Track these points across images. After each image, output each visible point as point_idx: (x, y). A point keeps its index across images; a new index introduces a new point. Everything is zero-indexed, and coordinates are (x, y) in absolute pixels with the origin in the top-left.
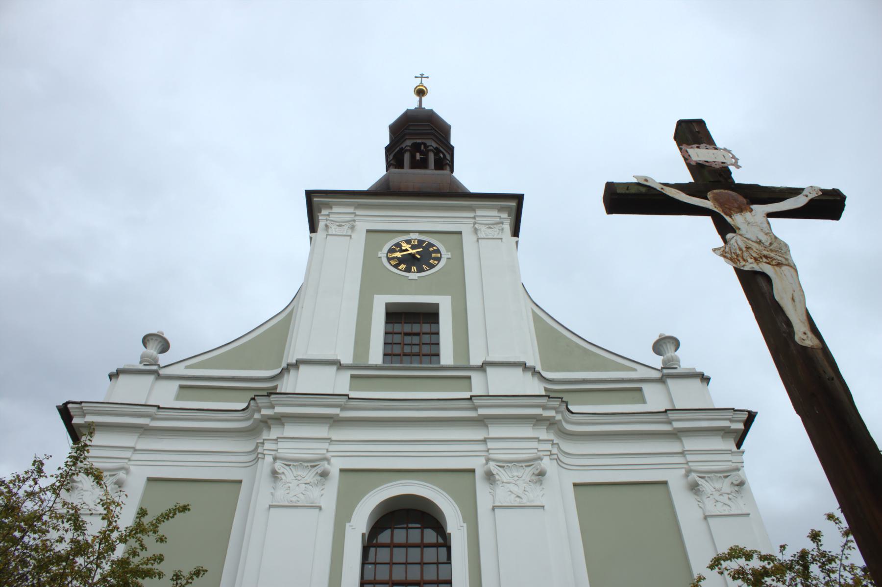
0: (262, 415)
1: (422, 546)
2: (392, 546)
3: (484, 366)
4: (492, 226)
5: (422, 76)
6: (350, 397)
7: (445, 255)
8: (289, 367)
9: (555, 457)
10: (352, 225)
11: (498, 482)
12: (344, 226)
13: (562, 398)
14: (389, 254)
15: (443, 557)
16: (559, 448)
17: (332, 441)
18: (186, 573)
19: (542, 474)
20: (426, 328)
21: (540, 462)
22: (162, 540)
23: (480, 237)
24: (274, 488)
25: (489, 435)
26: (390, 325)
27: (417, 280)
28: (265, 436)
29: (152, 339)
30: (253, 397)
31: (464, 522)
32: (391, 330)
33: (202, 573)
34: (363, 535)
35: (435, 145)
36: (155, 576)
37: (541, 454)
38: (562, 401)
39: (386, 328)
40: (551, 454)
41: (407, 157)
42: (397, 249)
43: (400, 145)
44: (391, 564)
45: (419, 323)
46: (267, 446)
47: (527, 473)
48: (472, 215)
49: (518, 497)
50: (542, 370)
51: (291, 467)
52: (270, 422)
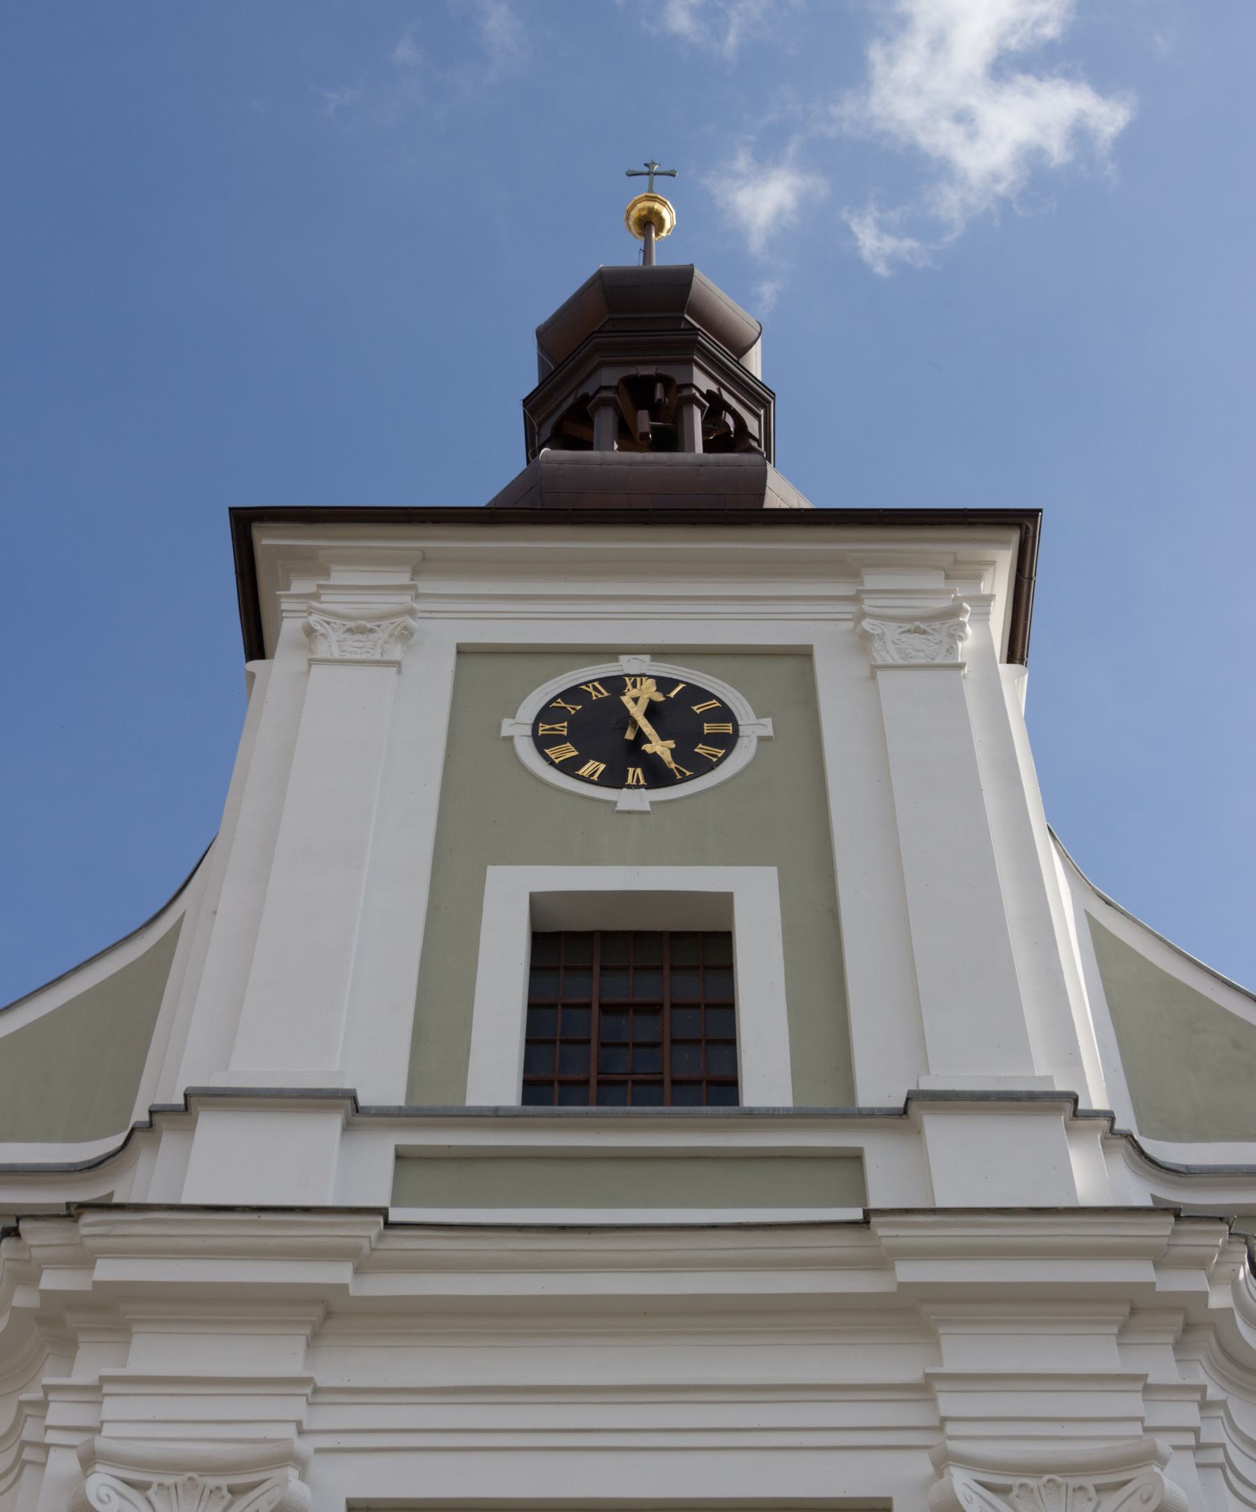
0: (45, 1294)
3: (913, 1106)
9: (1218, 1456)
12: (371, 631)
17: (317, 1391)
23: (880, 662)
27: (646, 813)
43: (576, 388)
46: (59, 1413)
51: (150, 1493)
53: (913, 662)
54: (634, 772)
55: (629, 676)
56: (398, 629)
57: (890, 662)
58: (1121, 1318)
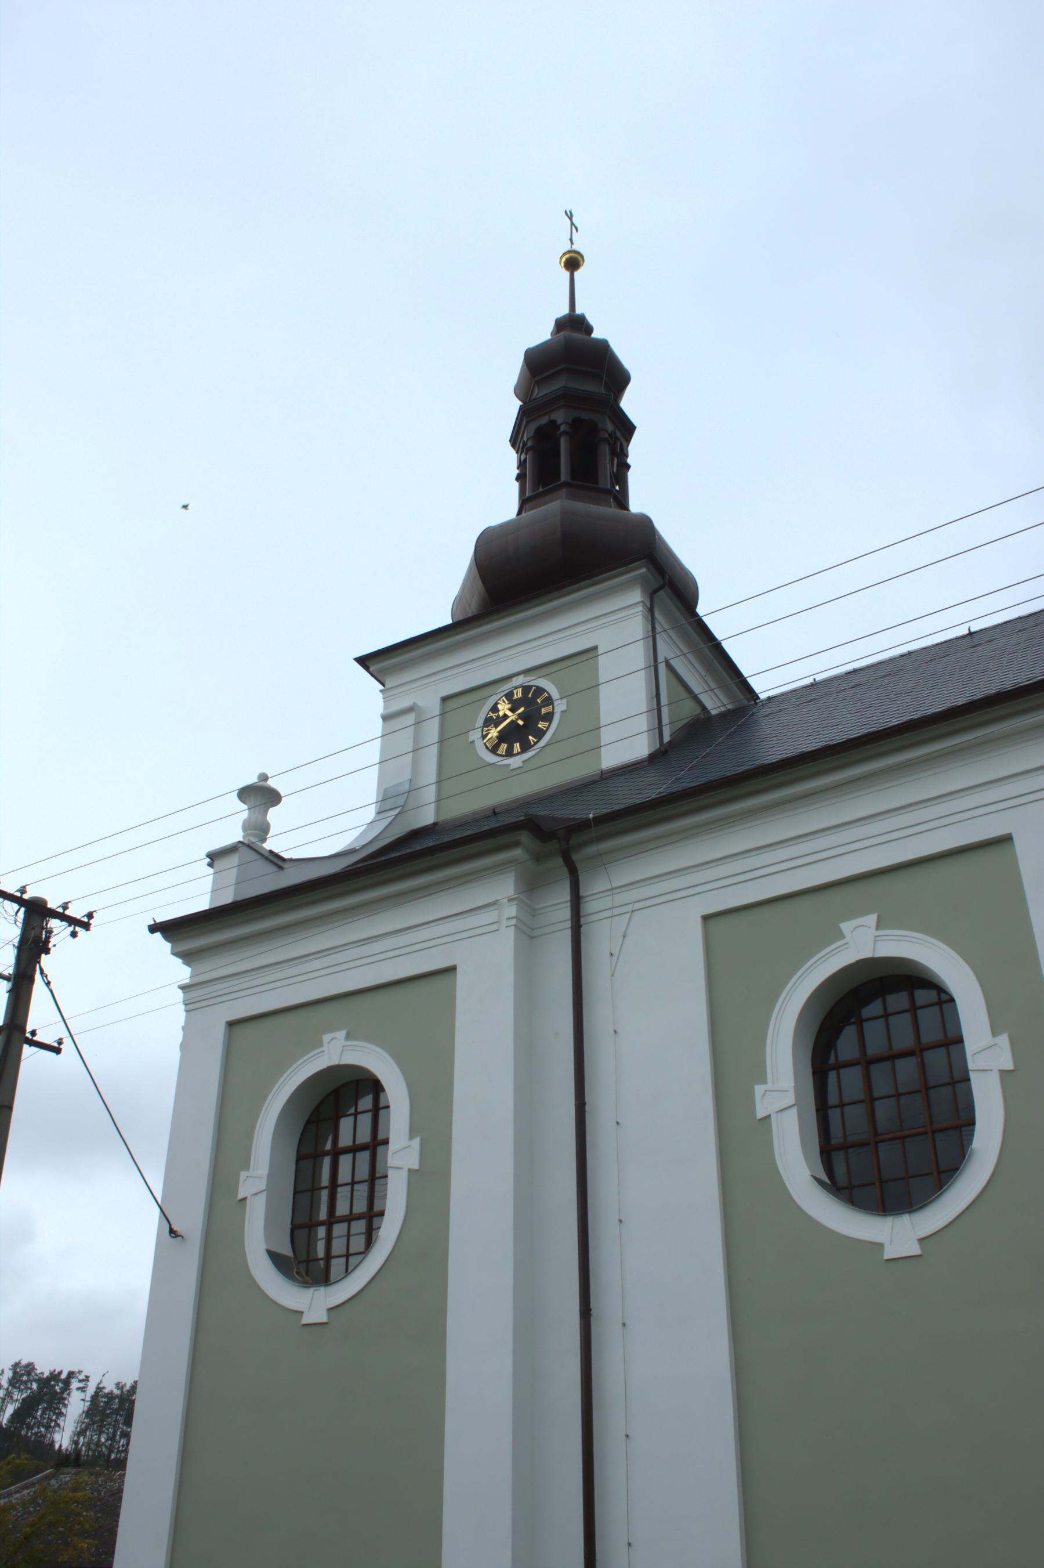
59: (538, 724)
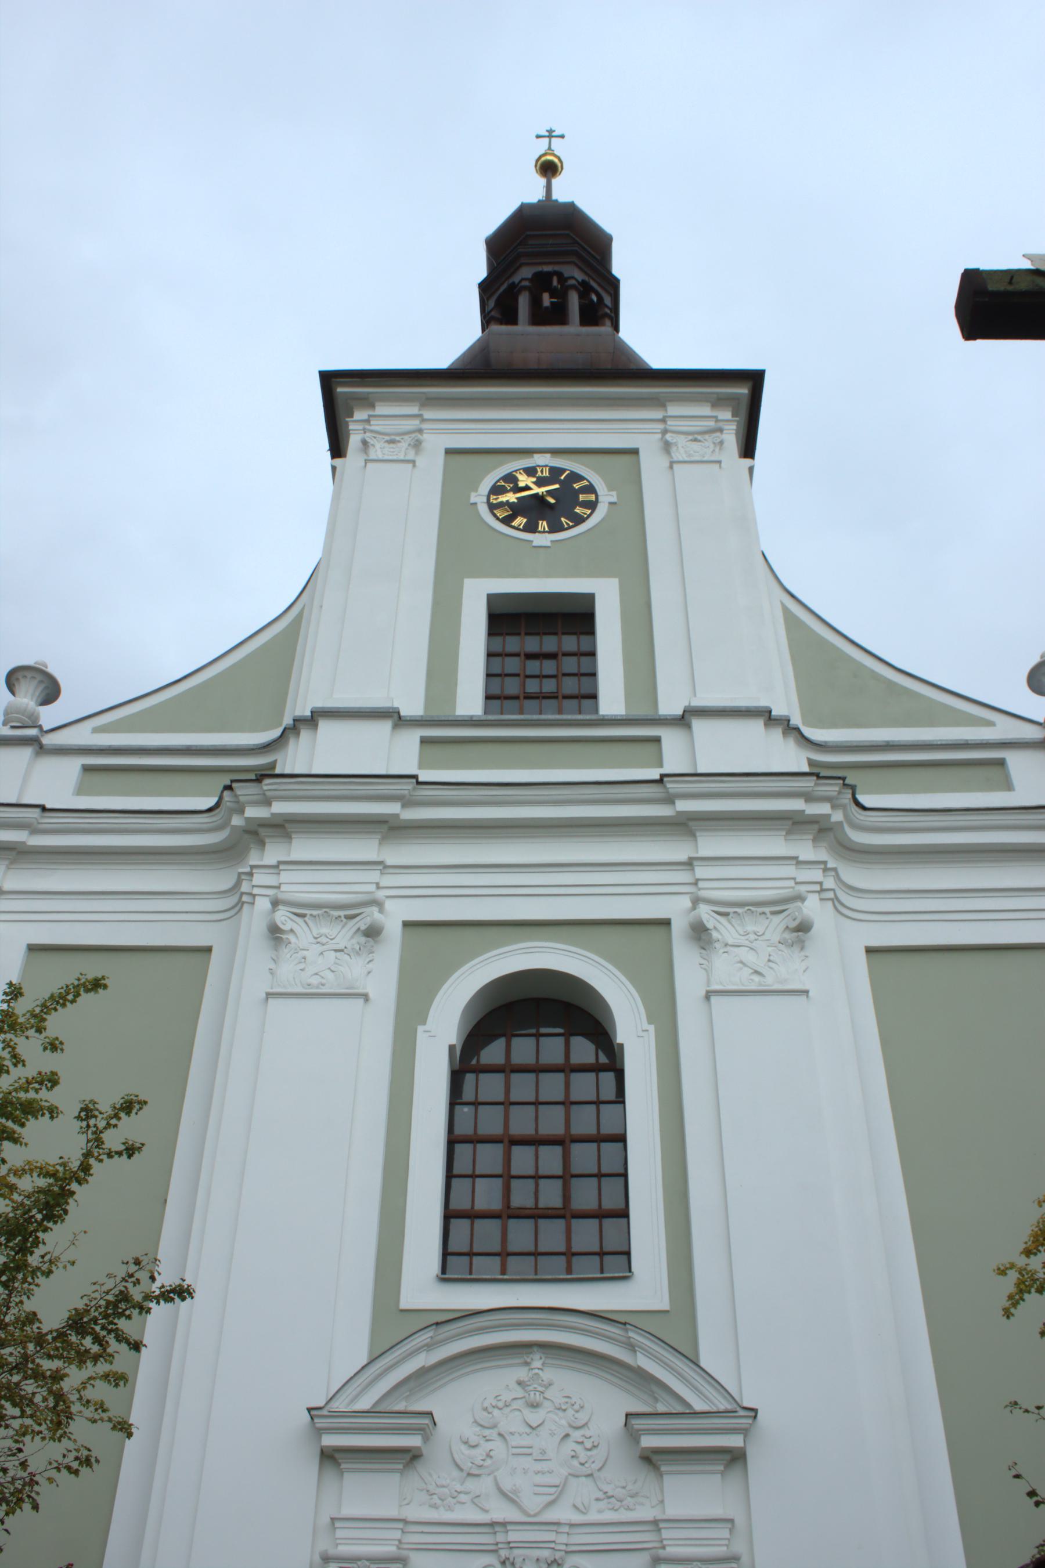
0: (248, 819)
1: (568, 1069)
2: (508, 1069)
3: (687, 716)
4: (699, 437)
5: (550, 135)
6: (421, 779)
7: (606, 496)
8: (296, 723)
9: (831, 895)
10: (417, 440)
11: (717, 945)
13: (844, 779)
14: (492, 497)
15: (608, 1091)
16: (838, 878)
17: (386, 867)
18: (105, 1106)
19: (803, 928)
20: (569, 643)
21: (799, 904)
22: (54, 1046)
23: (675, 459)
24: (274, 960)
25: (697, 852)
26: (498, 640)
28: (254, 859)
29: (25, 677)
30: (229, 783)
31: (650, 1023)
32: (498, 648)
33: (137, 1106)
34: (452, 1048)
35: (580, 276)
36: (43, 1115)
37: (803, 888)
38: (844, 785)
39: (489, 644)
40: (822, 890)
41: (523, 303)
42: (509, 486)
44: (507, 1103)
45: (555, 634)
46: (259, 878)
47: (775, 927)
48: (658, 414)
49: (756, 972)
50: (804, 724)
51: (306, 919)
52: (263, 832)
53: (693, 459)
54: (542, 524)
55: (539, 466)
56: (413, 441)
57: (681, 459)
58: (787, 827)
59: (575, 508)
